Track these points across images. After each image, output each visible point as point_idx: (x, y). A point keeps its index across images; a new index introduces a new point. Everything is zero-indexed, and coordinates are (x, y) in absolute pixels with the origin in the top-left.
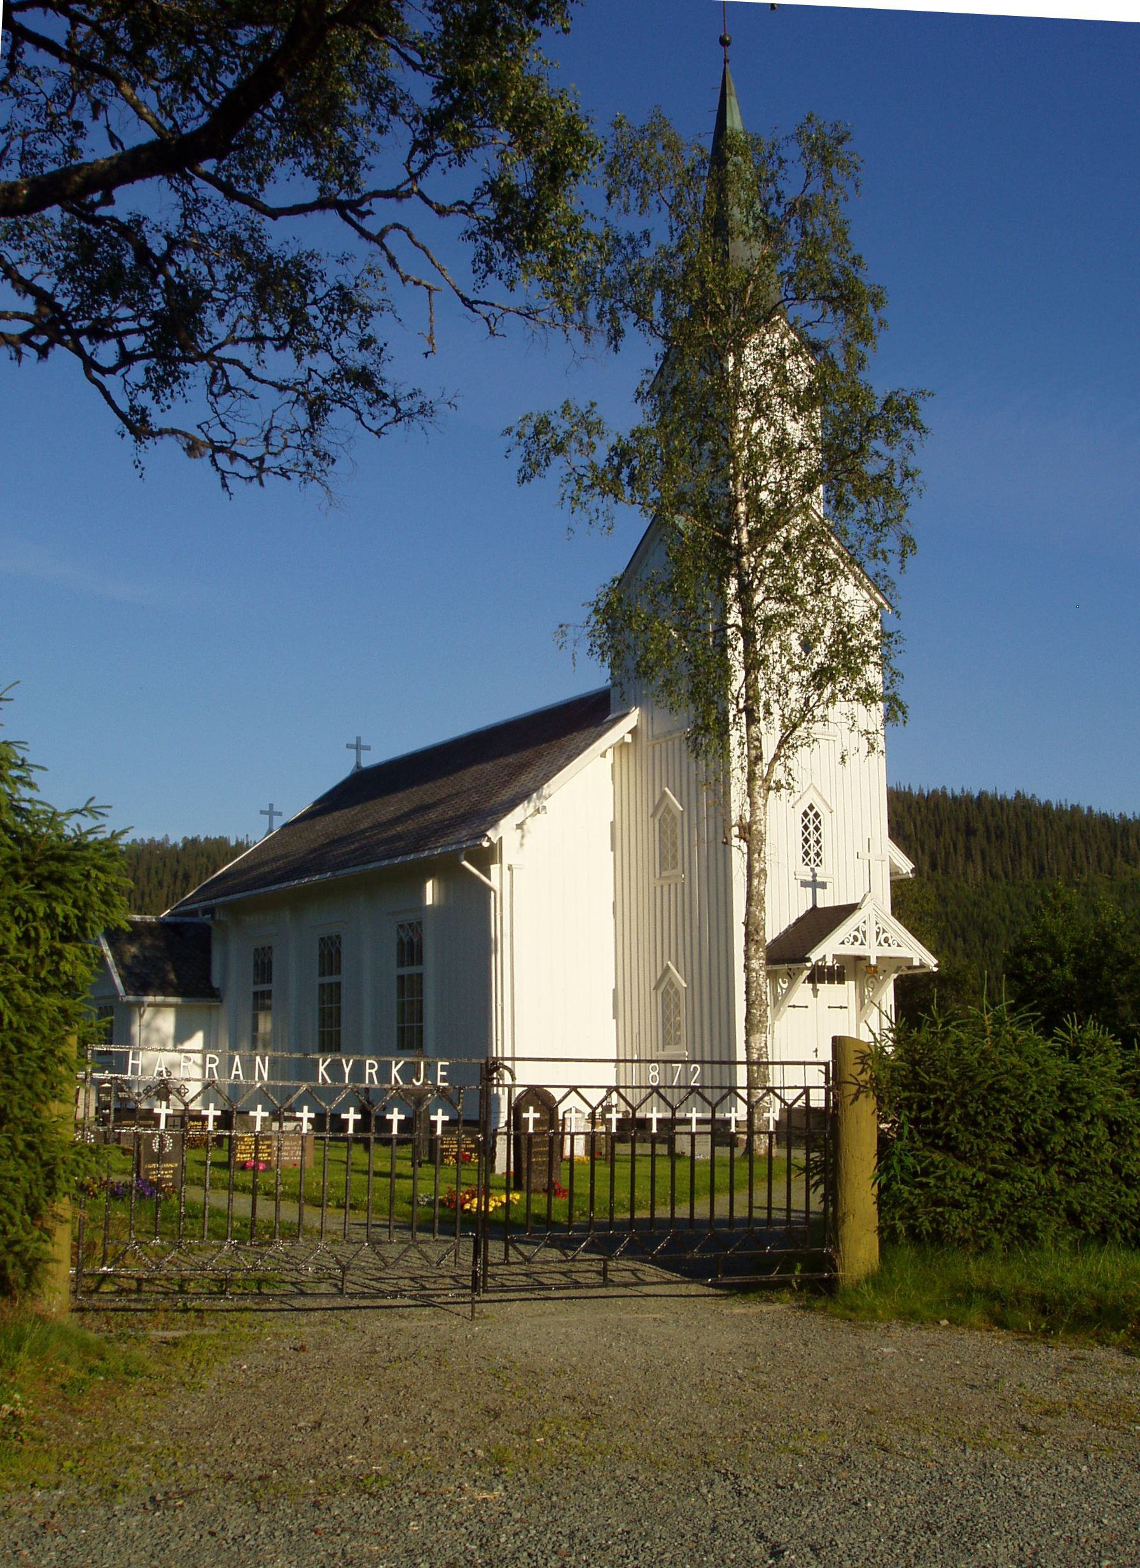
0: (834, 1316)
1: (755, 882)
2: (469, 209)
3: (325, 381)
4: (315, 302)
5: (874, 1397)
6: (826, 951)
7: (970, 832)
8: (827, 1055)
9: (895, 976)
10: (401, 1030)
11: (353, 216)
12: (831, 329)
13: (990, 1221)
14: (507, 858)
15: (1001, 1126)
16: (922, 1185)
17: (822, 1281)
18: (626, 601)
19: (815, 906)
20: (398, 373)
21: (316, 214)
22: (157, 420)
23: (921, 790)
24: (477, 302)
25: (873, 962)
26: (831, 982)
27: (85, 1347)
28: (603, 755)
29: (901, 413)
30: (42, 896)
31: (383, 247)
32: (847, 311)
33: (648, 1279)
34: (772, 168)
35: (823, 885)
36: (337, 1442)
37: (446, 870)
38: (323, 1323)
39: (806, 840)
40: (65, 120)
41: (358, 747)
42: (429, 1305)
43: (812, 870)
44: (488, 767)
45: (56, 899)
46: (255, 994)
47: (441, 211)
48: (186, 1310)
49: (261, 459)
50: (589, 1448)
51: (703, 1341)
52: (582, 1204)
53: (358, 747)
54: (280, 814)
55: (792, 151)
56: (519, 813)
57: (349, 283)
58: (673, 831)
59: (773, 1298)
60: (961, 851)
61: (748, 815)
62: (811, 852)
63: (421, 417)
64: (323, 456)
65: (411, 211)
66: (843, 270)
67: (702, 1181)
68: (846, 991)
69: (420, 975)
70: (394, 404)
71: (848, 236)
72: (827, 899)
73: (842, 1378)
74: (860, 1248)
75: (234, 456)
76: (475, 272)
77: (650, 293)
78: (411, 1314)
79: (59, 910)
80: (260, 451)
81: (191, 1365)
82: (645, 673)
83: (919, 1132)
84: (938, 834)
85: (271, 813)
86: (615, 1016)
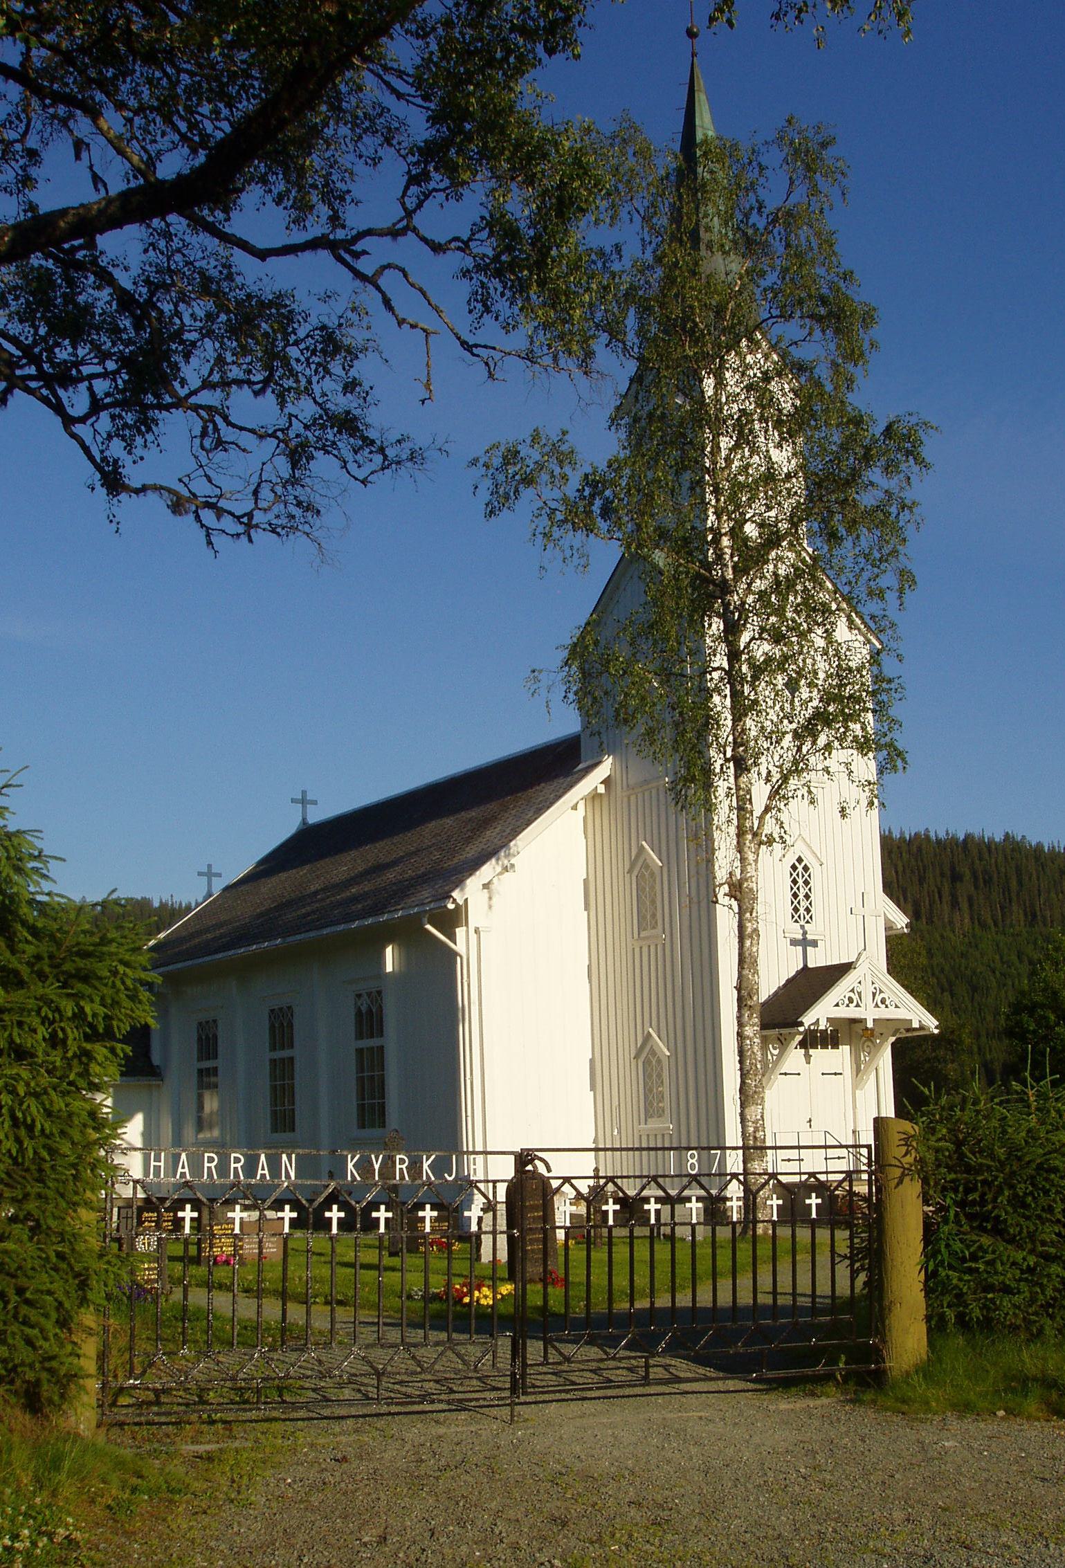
0: (887, 1409)
1: (748, 943)
2: (465, 247)
3: (306, 427)
4: (296, 343)
5: (945, 1494)
6: (820, 1014)
7: (956, 878)
8: (868, 1138)
9: (893, 1039)
10: (361, 1108)
11: (347, 257)
12: (817, 349)
13: (1042, 1306)
14: (473, 923)
15: (1050, 1206)
16: (971, 1271)
17: (870, 1372)
18: (602, 643)
19: (805, 966)
20: (381, 420)
21: (307, 255)
22: (133, 475)
23: (902, 833)
24: (476, 346)
25: (870, 1025)
26: (824, 1046)
27: (120, 1464)
28: (575, 808)
29: (902, 443)
30: (68, 995)
31: (378, 288)
32: (837, 331)
33: (682, 1375)
34: (752, 174)
35: (814, 944)
36: (407, 1557)
37: (408, 934)
38: (356, 1431)
39: (795, 896)
40: (18, 147)
41: (304, 801)
42: (465, 1409)
43: (802, 927)
44: (449, 821)
45: (83, 997)
46: (200, 1071)
47: (437, 248)
48: (213, 1422)
49: (250, 515)
50: (666, 1555)
51: (756, 1439)
52: (578, 1292)
53: (304, 801)
54: (219, 875)
55: (773, 157)
56: (488, 871)
57: (332, 322)
58: (652, 888)
59: (818, 1392)
60: (946, 897)
61: (738, 872)
62: (801, 907)
63: (409, 464)
64: (308, 508)
65: (407, 250)
66: (832, 286)
67: (704, 1266)
68: (840, 1057)
69: (381, 1048)
70: (382, 450)
71: (836, 248)
72: (817, 959)
73: (908, 1474)
74: (908, 1338)
75: (220, 513)
76: (470, 312)
77: (624, 312)
78: (446, 1419)
79: (88, 1009)
80: (248, 506)
81: (233, 1481)
82: (626, 721)
83: (968, 1216)
84: (921, 880)
85: (209, 874)
86: (593, 1088)
